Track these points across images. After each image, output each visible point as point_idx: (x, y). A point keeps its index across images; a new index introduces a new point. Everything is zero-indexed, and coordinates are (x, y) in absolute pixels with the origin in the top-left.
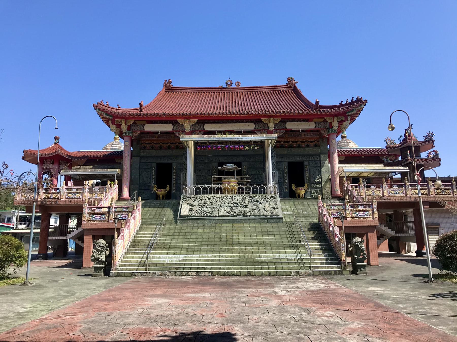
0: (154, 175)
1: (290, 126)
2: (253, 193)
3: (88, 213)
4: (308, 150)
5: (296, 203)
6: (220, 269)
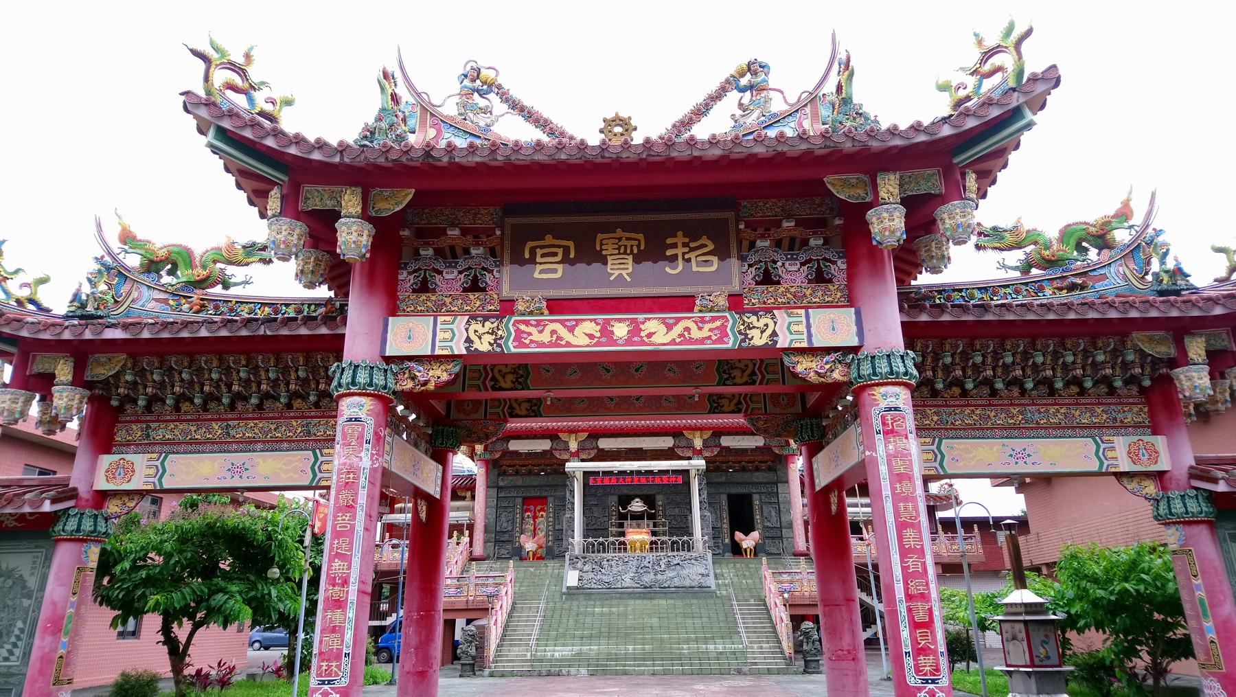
1: (726, 441)
2: (673, 550)
4: (759, 477)
5: (738, 565)
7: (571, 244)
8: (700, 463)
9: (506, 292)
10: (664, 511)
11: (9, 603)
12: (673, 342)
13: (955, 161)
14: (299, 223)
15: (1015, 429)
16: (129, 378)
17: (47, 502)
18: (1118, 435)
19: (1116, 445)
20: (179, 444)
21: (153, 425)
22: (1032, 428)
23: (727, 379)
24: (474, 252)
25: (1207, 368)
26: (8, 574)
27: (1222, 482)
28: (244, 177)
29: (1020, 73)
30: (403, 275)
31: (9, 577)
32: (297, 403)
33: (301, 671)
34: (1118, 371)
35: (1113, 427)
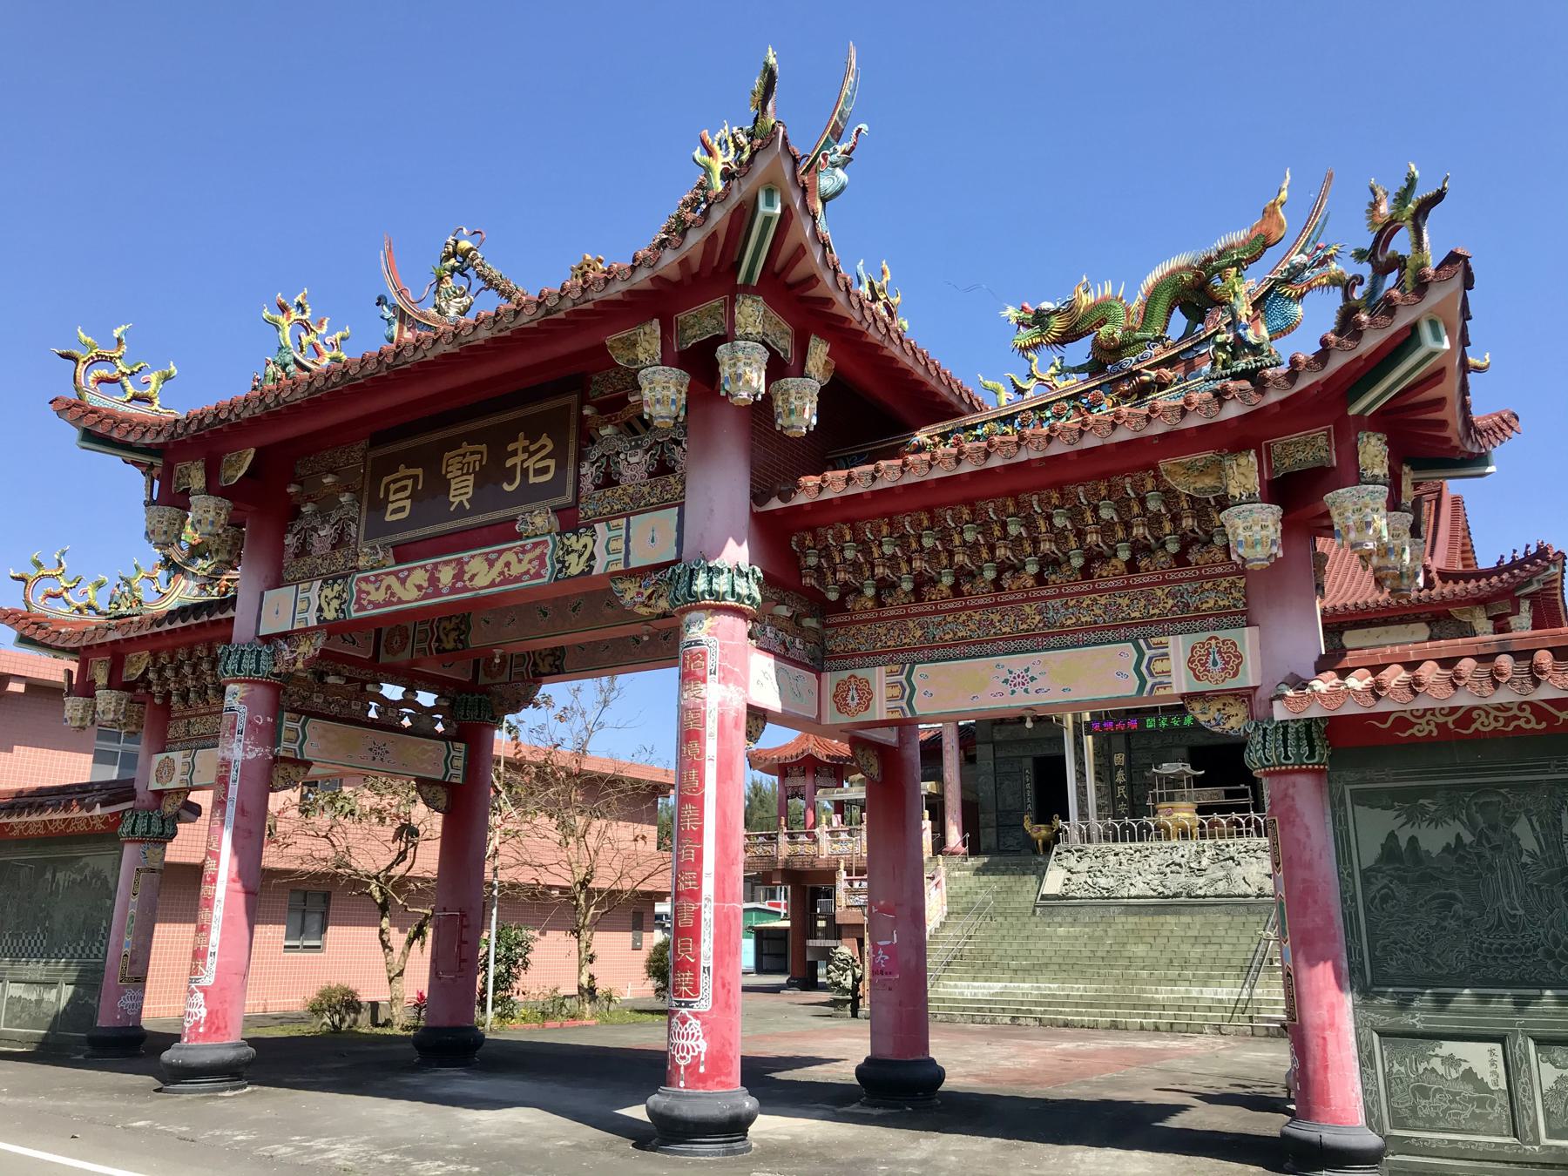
3: (846, 890)
6: (1060, 1013)
12: (493, 584)
19: (1170, 650)
22: (1053, 635)
33: (1478, 995)
35: (1180, 620)
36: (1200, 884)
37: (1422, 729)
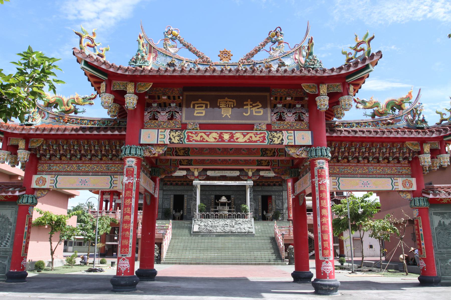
0: (172, 203)
2: (238, 218)
4: (275, 188)
7: (208, 103)
8: (250, 183)
9: (184, 121)
10: (234, 202)
11: (4, 227)
12: (246, 142)
13: (347, 81)
14: (112, 95)
15: (365, 174)
16: (44, 147)
17: (17, 192)
18: (400, 177)
20: (62, 172)
21: (52, 165)
22: (371, 174)
23: (265, 154)
24: (172, 105)
25: (430, 155)
26: (3, 217)
27: (431, 195)
28: (91, 77)
29: (369, 52)
30: (146, 113)
31: (3, 218)
32: (104, 158)
34: (401, 155)
35: (398, 175)
36: (233, 230)
37: (445, 201)
